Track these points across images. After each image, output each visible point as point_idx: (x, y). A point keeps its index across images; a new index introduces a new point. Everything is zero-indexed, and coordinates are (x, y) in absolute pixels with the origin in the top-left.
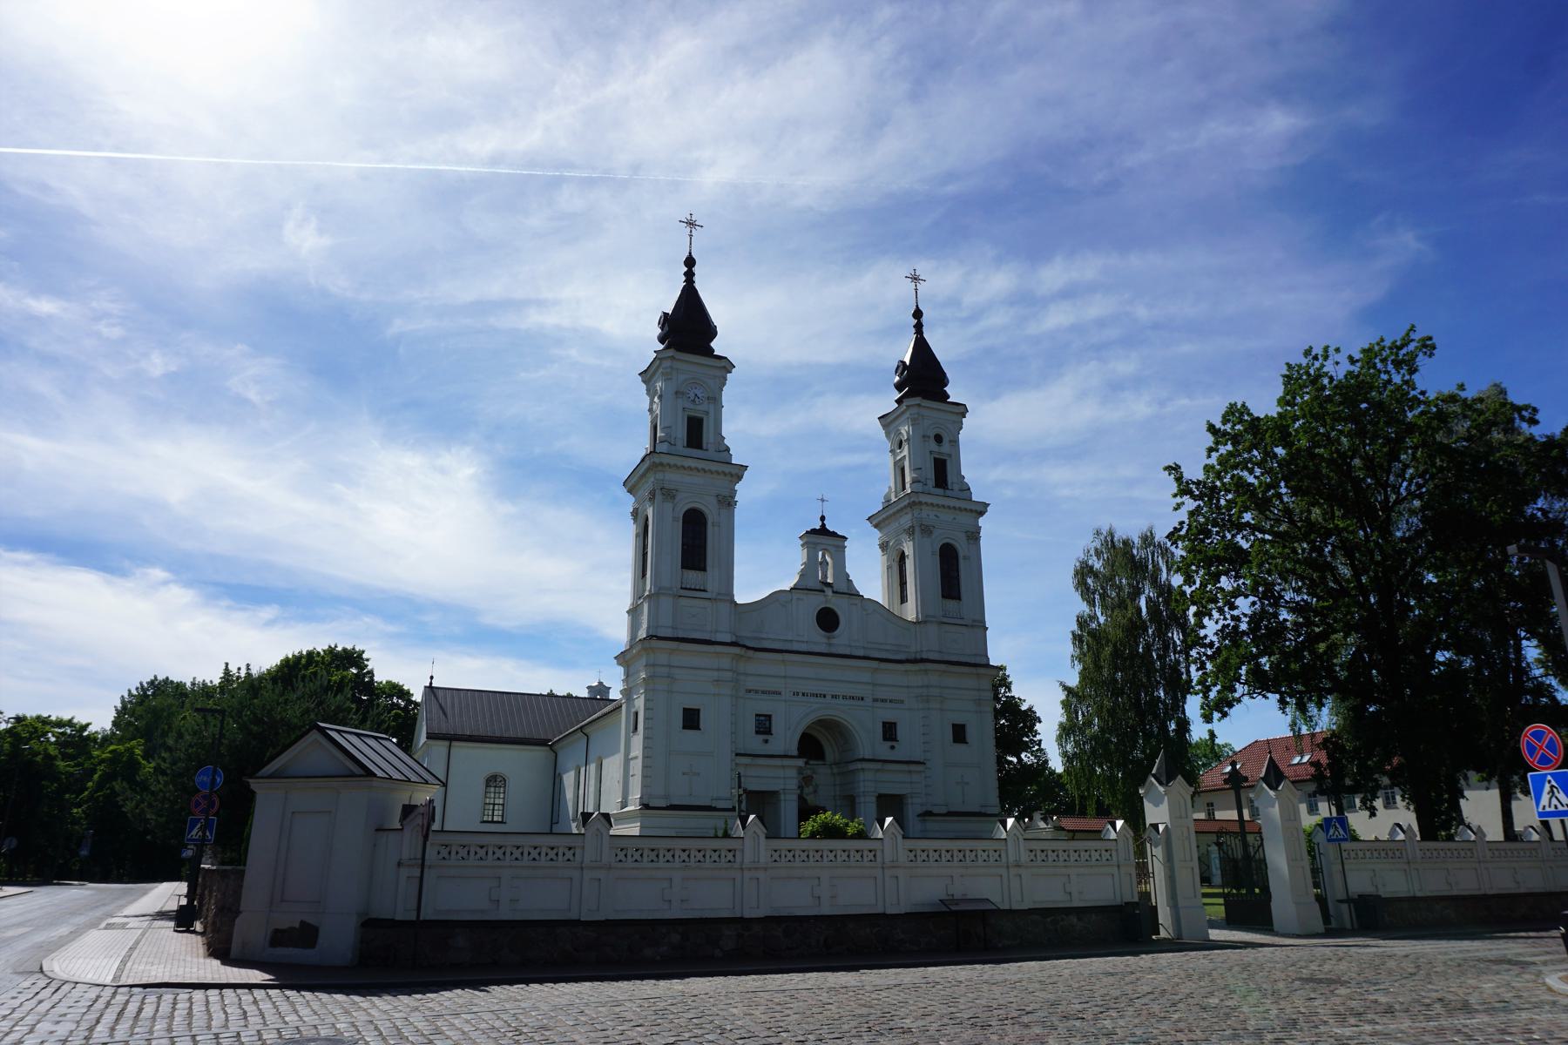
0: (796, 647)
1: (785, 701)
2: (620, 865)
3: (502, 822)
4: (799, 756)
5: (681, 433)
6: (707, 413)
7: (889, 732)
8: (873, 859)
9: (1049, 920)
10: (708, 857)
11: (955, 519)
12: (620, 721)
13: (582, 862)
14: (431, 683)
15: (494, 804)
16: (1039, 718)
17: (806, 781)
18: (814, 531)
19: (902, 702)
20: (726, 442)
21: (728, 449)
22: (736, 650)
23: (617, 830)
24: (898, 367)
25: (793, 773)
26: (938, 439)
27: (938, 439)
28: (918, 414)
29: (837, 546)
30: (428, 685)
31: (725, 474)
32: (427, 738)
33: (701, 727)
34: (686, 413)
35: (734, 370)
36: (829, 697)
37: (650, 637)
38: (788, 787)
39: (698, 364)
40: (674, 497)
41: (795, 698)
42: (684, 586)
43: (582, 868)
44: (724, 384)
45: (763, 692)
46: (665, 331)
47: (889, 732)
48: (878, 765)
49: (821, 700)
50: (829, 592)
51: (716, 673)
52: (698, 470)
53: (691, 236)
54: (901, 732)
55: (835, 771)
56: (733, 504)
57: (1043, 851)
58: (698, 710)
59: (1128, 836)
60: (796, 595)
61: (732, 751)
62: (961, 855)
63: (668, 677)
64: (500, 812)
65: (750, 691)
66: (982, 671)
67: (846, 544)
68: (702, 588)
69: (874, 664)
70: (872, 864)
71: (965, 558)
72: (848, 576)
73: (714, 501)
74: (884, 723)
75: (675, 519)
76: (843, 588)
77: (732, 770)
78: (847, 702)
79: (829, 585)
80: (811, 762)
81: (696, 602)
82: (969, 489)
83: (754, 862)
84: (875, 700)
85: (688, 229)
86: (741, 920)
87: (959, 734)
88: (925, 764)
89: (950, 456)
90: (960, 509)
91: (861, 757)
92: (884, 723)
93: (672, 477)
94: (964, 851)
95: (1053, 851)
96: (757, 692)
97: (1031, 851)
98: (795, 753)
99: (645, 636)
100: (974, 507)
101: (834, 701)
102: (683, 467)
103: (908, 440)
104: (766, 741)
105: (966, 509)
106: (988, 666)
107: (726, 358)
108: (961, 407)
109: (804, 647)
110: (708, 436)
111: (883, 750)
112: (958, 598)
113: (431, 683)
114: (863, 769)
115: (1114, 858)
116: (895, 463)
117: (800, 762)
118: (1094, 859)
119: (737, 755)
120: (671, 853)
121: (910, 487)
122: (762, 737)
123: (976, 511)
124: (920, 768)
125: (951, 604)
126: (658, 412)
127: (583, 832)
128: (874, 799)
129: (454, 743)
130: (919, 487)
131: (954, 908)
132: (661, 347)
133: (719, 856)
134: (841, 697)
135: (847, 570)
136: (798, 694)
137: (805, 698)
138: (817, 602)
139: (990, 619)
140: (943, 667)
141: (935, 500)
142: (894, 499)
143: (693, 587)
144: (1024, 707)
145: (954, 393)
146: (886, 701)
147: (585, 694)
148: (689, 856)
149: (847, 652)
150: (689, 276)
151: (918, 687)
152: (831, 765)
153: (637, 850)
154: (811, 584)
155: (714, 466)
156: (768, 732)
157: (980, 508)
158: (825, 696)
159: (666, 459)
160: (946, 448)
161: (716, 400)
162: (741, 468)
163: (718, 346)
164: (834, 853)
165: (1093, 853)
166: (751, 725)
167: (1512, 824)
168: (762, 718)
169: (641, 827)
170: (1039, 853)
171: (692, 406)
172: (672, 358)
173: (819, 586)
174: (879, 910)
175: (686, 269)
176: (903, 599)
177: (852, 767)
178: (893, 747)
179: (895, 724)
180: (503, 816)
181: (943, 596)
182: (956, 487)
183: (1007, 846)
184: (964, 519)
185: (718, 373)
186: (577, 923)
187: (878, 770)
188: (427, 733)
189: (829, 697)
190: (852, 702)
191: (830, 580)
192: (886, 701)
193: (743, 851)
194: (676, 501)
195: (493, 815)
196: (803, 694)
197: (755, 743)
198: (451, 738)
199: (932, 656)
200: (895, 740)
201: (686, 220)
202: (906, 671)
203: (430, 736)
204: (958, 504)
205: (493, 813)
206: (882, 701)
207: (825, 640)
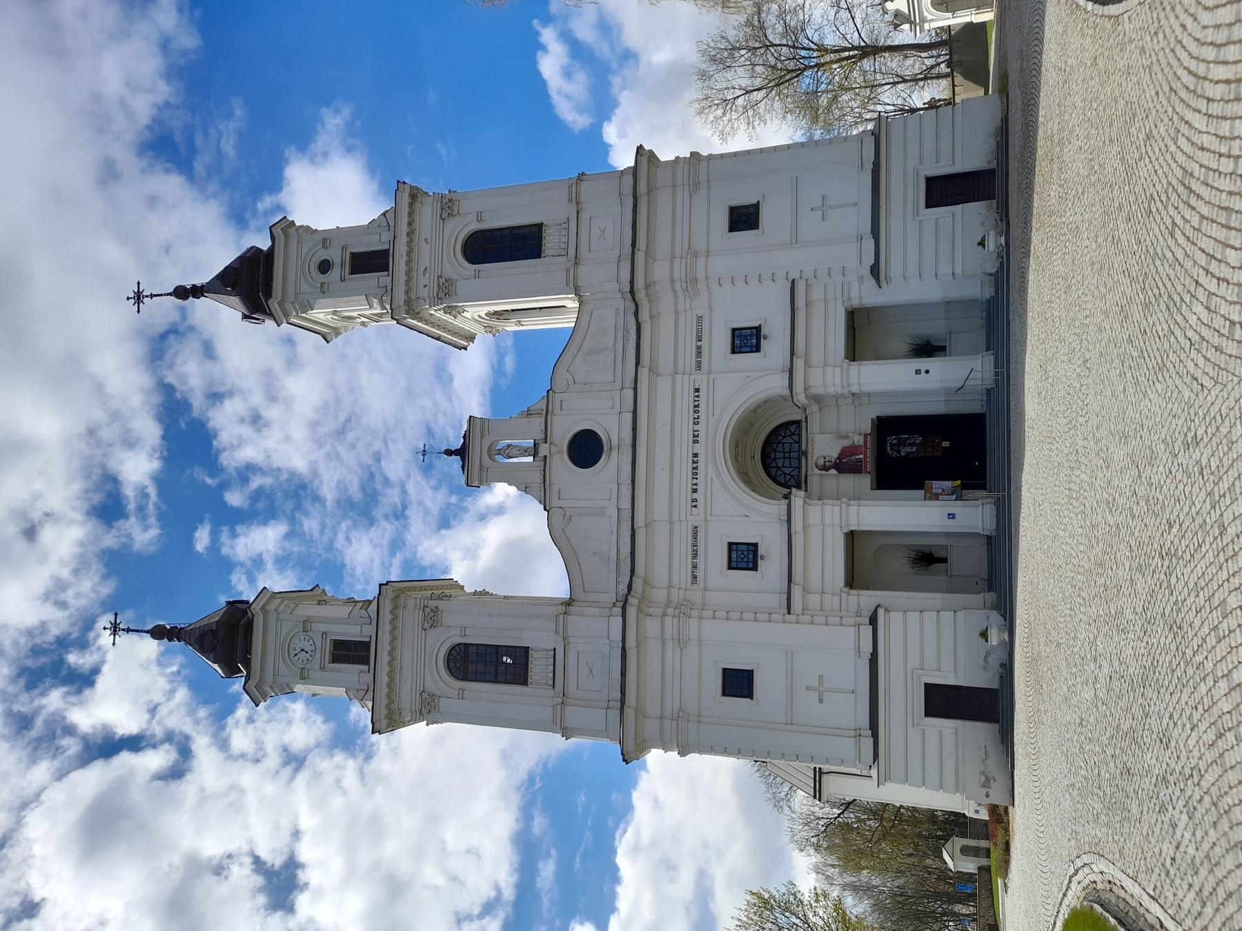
5: (352, 671)
6: (325, 634)
19: (700, 319)
22: (632, 611)
25: (815, 510)
26: (325, 267)
27: (325, 267)
29: (482, 425)
31: (395, 618)
33: (754, 201)
38: (837, 521)
39: (264, 634)
41: (700, 503)
44: (308, 228)
45: (695, 555)
48: (799, 364)
49: (701, 459)
51: (669, 643)
53: (152, 296)
65: (695, 577)
69: (644, 373)
73: (433, 635)
75: (477, 276)
78: (702, 414)
85: (145, 300)
88: (793, 281)
93: (425, 285)
96: (695, 567)
105: (410, 224)
109: (626, 491)
110: (372, 244)
125: (551, 241)
128: (854, 367)
134: (696, 428)
136: (694, 500)
137: (700, 488)
138: (562, 465)
140: (640, 257)
146: (699, 348)
149: (628, 417)
154: (537, 477)
160: (334, 255)
167: (873, 628)
171: (318, 655)
181: (539, 257)
187: (807, 364)
190: (702, 409)
192: (699, 348)
194: (456, 278)
196: (695, 491)
199: (625, 275)
201: (141, 290)
202: (651, 317)
206: (699, 353)
207: (614, 453)
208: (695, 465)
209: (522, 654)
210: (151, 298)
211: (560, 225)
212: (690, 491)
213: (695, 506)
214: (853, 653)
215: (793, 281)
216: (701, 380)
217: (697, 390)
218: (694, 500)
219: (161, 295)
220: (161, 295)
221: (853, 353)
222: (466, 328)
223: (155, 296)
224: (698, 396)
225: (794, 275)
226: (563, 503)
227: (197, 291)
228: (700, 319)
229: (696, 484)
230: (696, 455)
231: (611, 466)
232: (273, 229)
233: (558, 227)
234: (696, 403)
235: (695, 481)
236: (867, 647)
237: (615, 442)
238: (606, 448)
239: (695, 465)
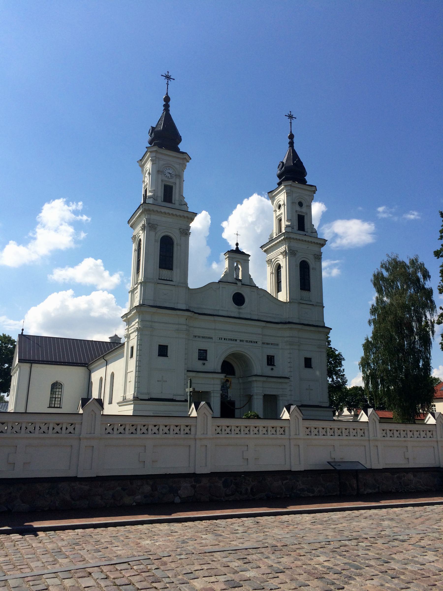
0: (221, 313)
1: (215, 342)
2: (109, 436)
3: (59, 407)
4: (222, 372)
5: (160, 193)
7: (271, 360)
8: (283, 433)
9: (396, 476)
10: (171, 430)
11: (308, 247)
12: (124, 352)
13: (80, 434)
14: (22, 333)
15: (55, 398)
16: (344, 358)
17: (225, 387)
18: (232, 251)
19: (277, 345)
20: (185, 200)
21: (186, 204)
23: (109, 410)
24: (280, 165)
26: (301, 204)
27: (301, 204)
28: (290, 190)
29: (245, 260)
30: (21, 334)
32: (19, 362)
34: (164, 183)
35: (190, 161)
36: (238, 341)
37: (140, 306)
40: (155, 229)
41: (220, 341)
42: (160, 278)
43: (80, 439)
44: (185, 168)
46: (152, 137)
47: (271, 360)
48: (264, 379)
49: (235, 342)
50: (239, 284)
52: (169, 214)
54: (277, 361)
55: (241, 381)
56: (188, 234)
57: (390, 430)
58: (167, 346)
59: (375, 419)
60: (221, 285)
61: (185, 369)
62: (340, 431)
63: (151, 327)
64: (59, 402)
65: (196, 337)
66: (321, 329)
67: (250, 258)
68: (170, 279)
69: (263, 324)
70: (283, 436)
71: (313, 269)
72: (250, 276)
74: (267, 356)
75: (156, 241)
76: (247, 282)
77: (185, 374)
79: (240, 280)
80: (228, 376)
81: (167, 287)
82: (316, 232)
83: (204, 434)
84: (263, 343)
86: (194, 475)
87: (308, 363)
88: (289, 378)
89: (307, 214)
90: (311, 242)
91: (255, 374)
92: (267, 356)
94: (342, 429)
95: (397, 431)
96: (199, 337)
97: (383, 430)
98: (220, 371)
99: (138, 304)
100: (319, 242)
101: (241, 343)
102: (161, 212)
103: (284, 204)
104: (204, 364)
106: (324, 327)
107: (186, 153)
108: (313, 187)
110: (175, 197)
111: (267, 370)
112: (309, 290)
113: (22, 333)
114: (256, 381)
115: (435, 436)
116: (276, 217)
117: (222, 376)
118: (422, 437)
119: (188, 371)
120: (146, 427)
121: (285, 230)
122: (201, 362)
123: (320, 244)
124: (286, 381)
126: (148, 182)
127: (81, 411)
128: (262, 397)
129: (34, 365)
130: (289, 230)
131: (338, 468)
132: (149, 145)
133: (180, 430)
135: (250, 273)
136: (222, 339)
137: (226, 341)
138: (233, 289)
139: (326, 302)
140: (300, 327)
141: (298, 237)
142: (275, 236)
143: (165, 279)
144: (337, 353)
145: (309, 179)
146: (269, 344)
147: (108, 340)
148: (158, 430)
149: (249, 317)
150: (167, 107)
151: (287, 337)
152: (238, 378)
153: (121, 425)
154: (230, 280)
155: (178, 213)
156: (205, 359)
157: (322, 242)
158: (236, 340)
159: (152, 207)
160: (304, 209)
161: (179, 176)
162: (194, 214)
163: (182, 147)
164: (257, 429)
165: (422, 433)
166: (196, 355)
168: (202, 351)
169: (134, 410)
170: (388, 431)
172: (156, 151)
173: (234, 281)
174: (287, 468)
175: (164, 103)
176: (279, 289)
177: (250, 379)
178: (272, 369)
179: (274, 356)
180: (60, 404)
182: (309, 231)
183: (368, 426)
184: (314, 248)
185: (181, 161)
186: (75, 479)
187: (264, 381)
188: (18, 359)
189: (238, 341)
191: (240, 278)
192: (269, 344)
193: (196, 426)
195: (55, 404)
196: (225, 339)
197: (198, 365)
198: (32, 362)
200: (274, 365)
203: (20, 361)
204: (310, 239)
205: (55, 403)
208: (233, 340)
209: (170, 268)
210: (290, 123)
211: (309, 298)
212: (225, 337)
213: (220, 339)
214: (175, 393)
215: (289, 378)
216: (260, 344)
217: (256, 342)
218: (222, 339)
219: (291, 127)
220: (291, 127)
221: (265, 396)
222: (272, 253)
223: (291, 124)
224: (255, 343)
225: (292, 379)
226: (221, 289)
227: (291, 144)
228: (277, 345)
229: (227, 340)
230: (236, 340)
231: (233, 309)
232: (315, 187)
233: (309, 297)
234: (252, 342)
235: (228, 339)
236: (178, 398)
237: (241, 311)
238: (240, 307)
239: (233, 340)
